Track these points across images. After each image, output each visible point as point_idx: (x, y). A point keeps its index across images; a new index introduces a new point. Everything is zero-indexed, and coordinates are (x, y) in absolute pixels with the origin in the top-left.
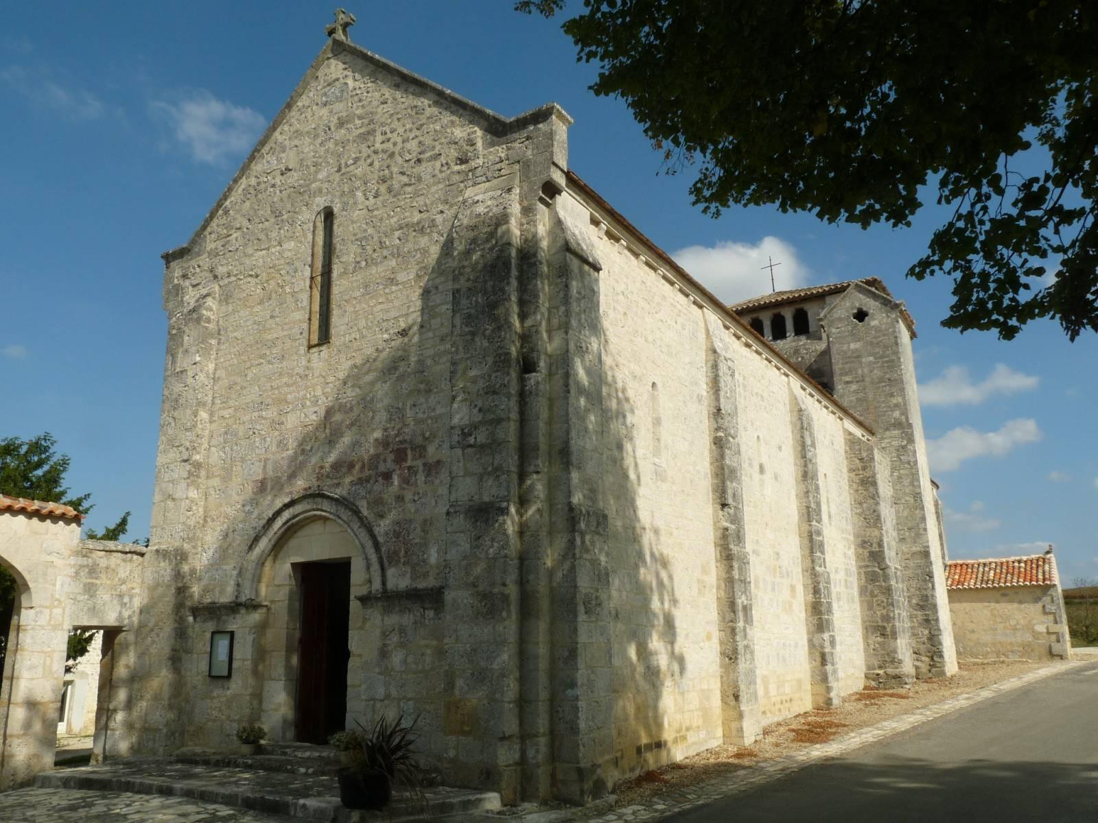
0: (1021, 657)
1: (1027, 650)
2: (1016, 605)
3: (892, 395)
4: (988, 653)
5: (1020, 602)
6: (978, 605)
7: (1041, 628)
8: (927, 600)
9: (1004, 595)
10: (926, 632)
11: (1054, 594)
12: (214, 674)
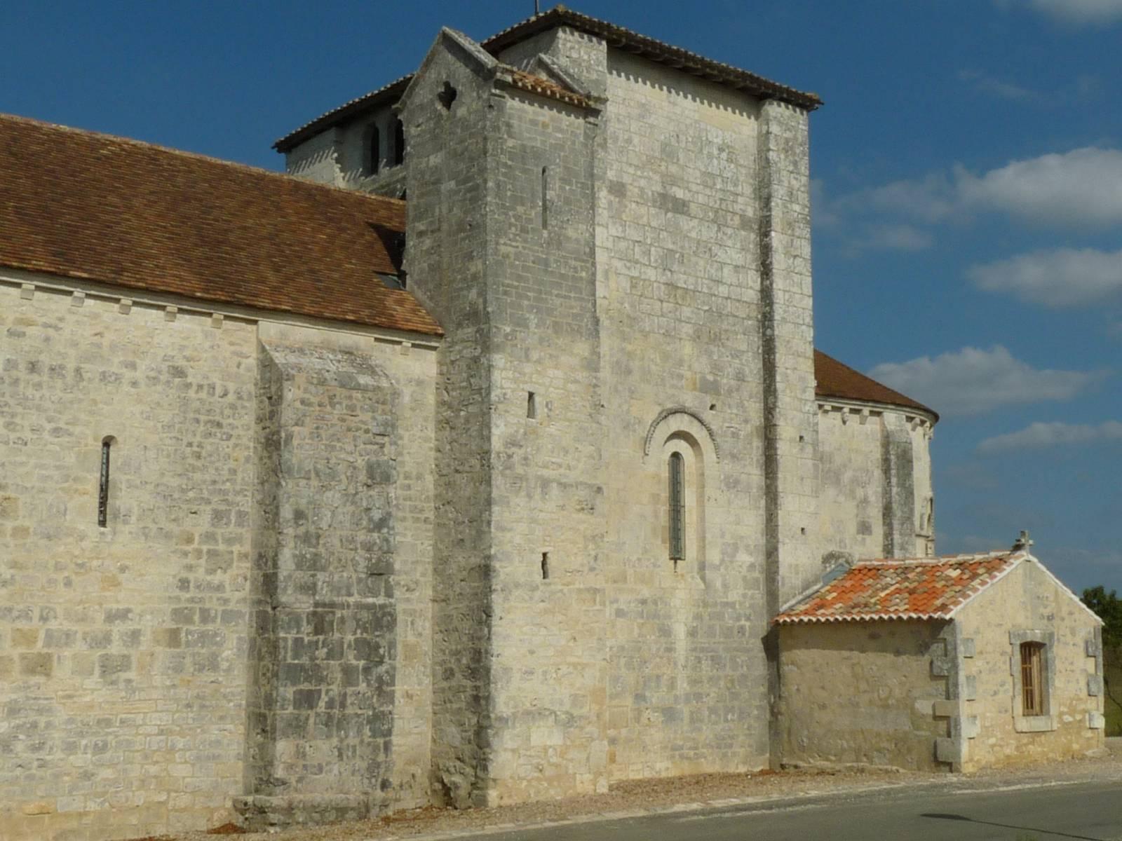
0: (891, 762)
1: (900, 748)
2: (890, 657)
3: (470, 257)
4: (843, 750)
5: (898, 653)
6: (833, 655)
7: (924, 707)
8: (479, 661)
9: (873, 637)
10: (474, 720)
11: (949, 638)
12: (937, 714)
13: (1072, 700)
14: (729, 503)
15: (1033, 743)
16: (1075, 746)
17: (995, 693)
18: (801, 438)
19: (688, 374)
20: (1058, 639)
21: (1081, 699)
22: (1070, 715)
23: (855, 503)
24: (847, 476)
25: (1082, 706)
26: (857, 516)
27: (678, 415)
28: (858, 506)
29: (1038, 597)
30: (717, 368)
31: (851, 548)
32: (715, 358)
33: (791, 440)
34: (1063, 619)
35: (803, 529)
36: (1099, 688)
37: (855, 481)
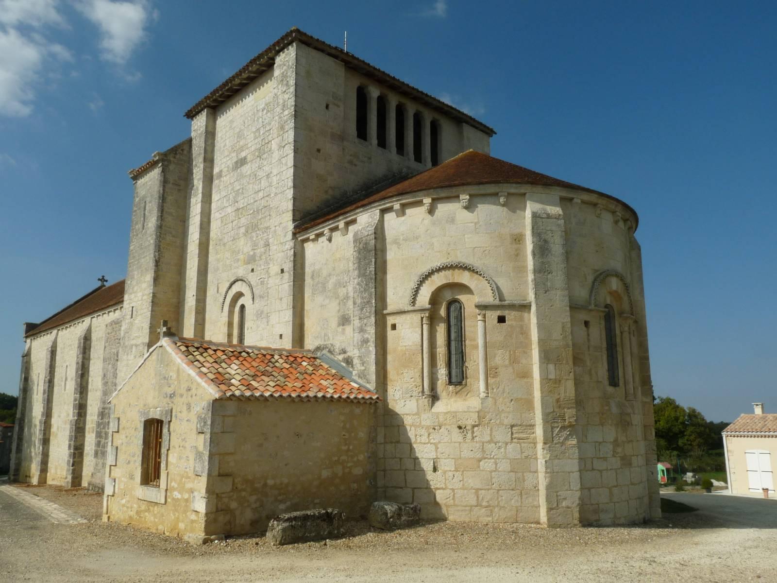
13: (182, 477)
15: (148, 510)
20: (176, 417)
21: (189, 478)
22: (179, 493)
23: (338, 301)
24: (330, 285)
25: (189, 485)
26: (339, 311)
27: (236, 283)
28: (339, 304)
29: (165, 378)
30: (255, 246)
31: (333, 339)
32: (254, 239)
33: (277, 274)
34: (182, 396)
35: (281, 336)
36: (203, 467)
37: (340, 284)
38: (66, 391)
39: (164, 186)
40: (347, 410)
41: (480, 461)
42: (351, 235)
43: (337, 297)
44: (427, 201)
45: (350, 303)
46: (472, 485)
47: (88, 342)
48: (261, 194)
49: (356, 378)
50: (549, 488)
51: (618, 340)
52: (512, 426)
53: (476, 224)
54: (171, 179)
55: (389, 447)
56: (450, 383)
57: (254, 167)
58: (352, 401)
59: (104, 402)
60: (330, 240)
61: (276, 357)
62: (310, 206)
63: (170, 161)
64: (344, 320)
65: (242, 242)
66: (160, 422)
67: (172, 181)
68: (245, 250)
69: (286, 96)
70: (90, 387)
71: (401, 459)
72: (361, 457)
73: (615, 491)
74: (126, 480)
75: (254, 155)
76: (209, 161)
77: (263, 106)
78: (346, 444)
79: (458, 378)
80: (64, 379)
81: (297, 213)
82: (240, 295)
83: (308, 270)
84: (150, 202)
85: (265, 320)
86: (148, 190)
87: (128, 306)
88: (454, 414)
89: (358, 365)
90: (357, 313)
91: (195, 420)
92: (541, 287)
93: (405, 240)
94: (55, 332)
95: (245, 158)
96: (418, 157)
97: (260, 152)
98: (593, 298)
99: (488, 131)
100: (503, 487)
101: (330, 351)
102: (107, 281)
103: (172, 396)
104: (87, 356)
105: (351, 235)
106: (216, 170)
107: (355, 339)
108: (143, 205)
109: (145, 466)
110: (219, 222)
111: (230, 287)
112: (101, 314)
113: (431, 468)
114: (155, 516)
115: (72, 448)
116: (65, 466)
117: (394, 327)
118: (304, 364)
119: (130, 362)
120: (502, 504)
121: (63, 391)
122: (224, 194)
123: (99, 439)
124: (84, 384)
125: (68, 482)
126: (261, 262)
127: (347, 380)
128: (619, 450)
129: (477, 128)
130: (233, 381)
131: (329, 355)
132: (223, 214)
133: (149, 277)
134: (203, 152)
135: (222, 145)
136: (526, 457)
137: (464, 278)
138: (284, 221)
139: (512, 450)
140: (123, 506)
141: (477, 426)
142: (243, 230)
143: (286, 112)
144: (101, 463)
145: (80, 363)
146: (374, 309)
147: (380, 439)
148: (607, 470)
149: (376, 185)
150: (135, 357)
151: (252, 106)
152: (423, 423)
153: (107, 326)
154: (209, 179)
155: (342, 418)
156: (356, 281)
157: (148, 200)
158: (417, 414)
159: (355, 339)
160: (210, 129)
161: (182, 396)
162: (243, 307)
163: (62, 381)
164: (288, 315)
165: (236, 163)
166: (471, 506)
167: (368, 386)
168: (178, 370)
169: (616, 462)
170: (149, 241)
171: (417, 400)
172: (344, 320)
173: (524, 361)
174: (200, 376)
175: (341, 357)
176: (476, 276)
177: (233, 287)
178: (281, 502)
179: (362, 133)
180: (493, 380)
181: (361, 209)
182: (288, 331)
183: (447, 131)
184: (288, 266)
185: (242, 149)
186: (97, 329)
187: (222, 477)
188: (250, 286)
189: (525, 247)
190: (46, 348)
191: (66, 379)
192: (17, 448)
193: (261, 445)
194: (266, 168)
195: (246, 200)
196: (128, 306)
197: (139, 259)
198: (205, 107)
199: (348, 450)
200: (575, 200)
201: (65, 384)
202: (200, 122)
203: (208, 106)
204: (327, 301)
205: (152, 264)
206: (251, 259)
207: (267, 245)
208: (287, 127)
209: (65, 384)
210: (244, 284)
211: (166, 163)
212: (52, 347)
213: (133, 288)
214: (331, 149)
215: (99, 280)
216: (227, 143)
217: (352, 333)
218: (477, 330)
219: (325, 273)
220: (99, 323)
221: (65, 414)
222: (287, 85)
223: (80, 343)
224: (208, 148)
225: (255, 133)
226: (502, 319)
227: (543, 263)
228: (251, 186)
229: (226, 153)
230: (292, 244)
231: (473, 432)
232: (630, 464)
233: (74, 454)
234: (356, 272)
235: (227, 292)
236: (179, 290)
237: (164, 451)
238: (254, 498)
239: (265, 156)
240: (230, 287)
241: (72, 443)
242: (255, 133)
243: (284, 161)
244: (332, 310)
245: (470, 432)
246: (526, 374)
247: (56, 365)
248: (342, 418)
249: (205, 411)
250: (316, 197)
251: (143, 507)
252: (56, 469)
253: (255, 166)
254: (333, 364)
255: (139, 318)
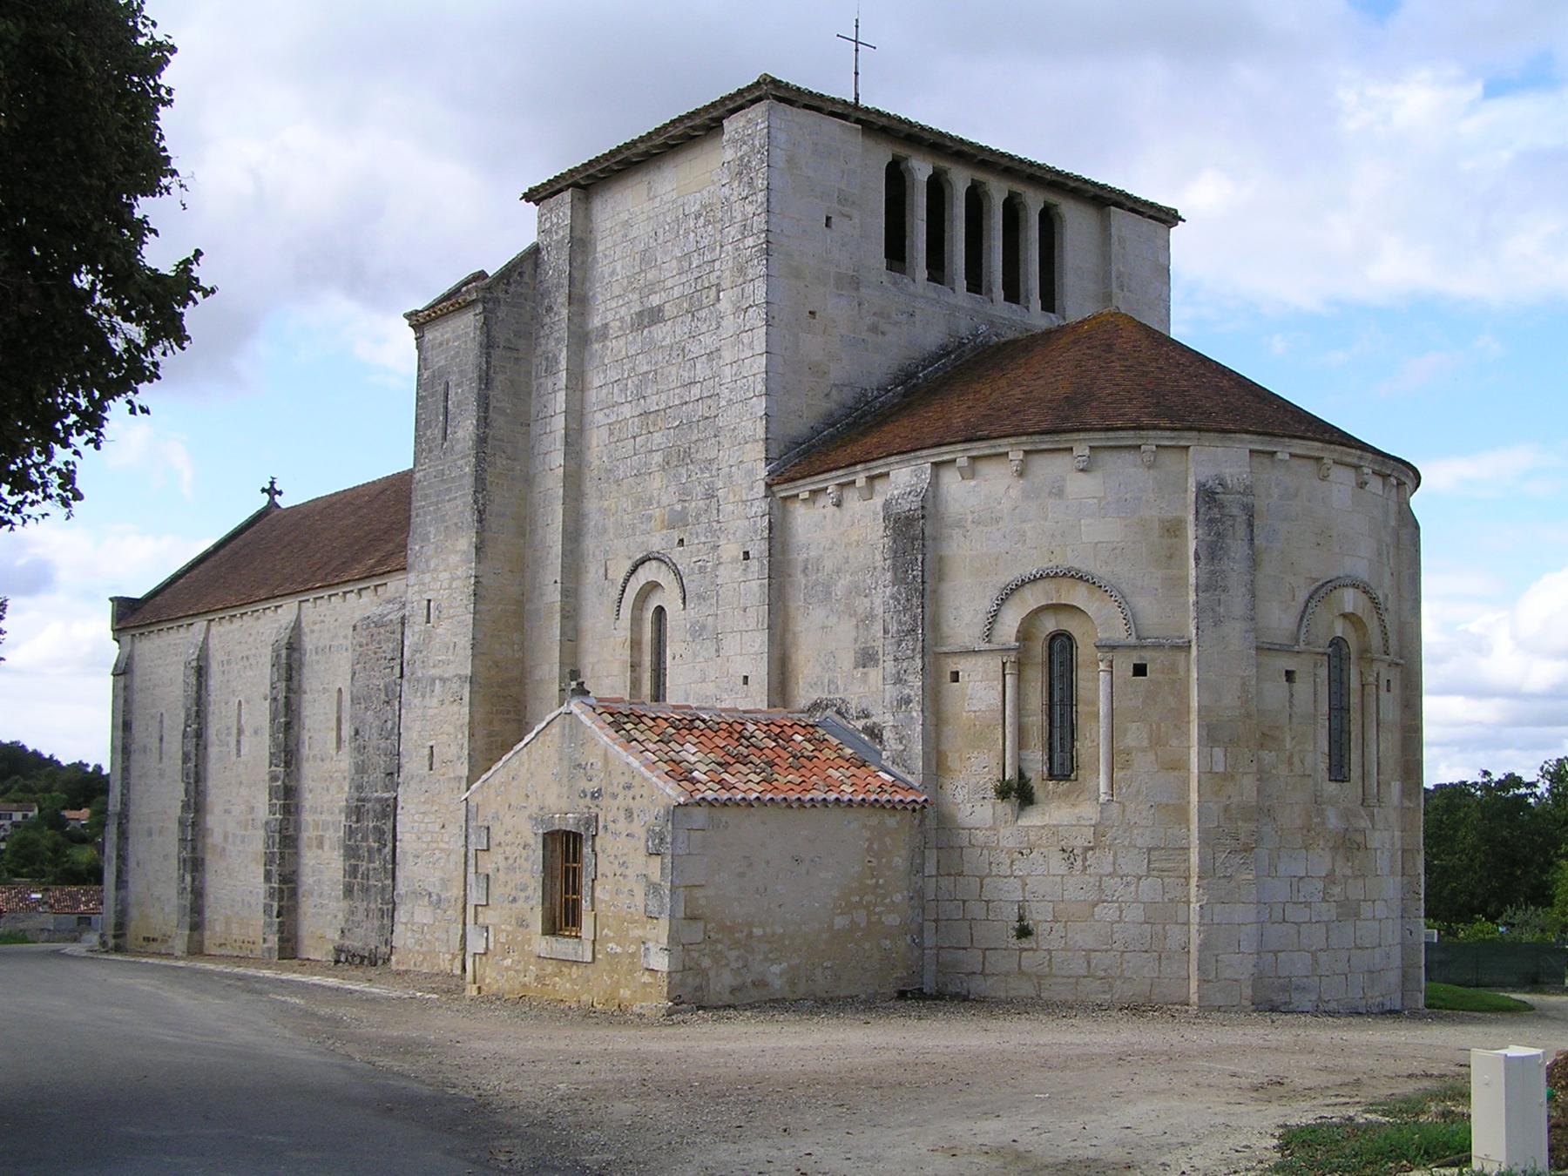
14: (695, 655)
15: (560, 974)
16: (625, 993)
17: (514, 900)
18: (746, 554)
19: (657, 512)
20: (605, 827)
25: (638, 932)
26: (856, 640)
30: (685, 494)
33: (734, 560)
34: (615, 796)
36: (662, 905)
37: (856, 590)
38: (243, 758)
39: (488, 355)
40: (873, 821)
41: (1095, 905)
42: (878, 501)
43: (853, 614)
44: (1016, 455)
45: (877, 628)
46: (1080, 943)
47: (296, 655)
48: (696, 391)
49: (888, 764)
50: (1203, 947)
51: (1355, 700)
52: (1150, 850)
53: (1100, 499)
54: (501, 337)
55: (945, 882)
56: (1051, 776)
57: (678, 332)
58: (883, 807)
59: (360, 788)
60: (838, 505)
61: (751, 727)
62: (799, 426)
63: (497, 301)
64: (867, 658)
65: (657, 482)
66: (577, 837)
67: (502, 344)
68: (665, 500)
69: (750, 209)
70: (305, 751)
71: (964, 902)
72: (898, 898)
73: (1322, 956)
74: (509, 928)
75: (679, 306)
76: (579, 301)
77: (697, 207)
78: (873, 876)
79: (1063, 767)
80: (234, 731)
81: (773, 445)
82: (653, 586)
83: (799, 557)
84: (458, 385)
85: (711, 647)
86: (453, 358)
87: (416, 598)
88: (1055, 829)
89: (892, 742)
90: (889, 648)
91: (641, 833)
92: (1209, 614)
93: (976, 523)
94: (200, 624)
95: (660, 309)
96: (1013, 292)
97: (691, 304)
98: (1304, 630)
99: (1164, 217)
100: (1131, 948)
101: (838, 712)
102: (280, 493)
103: (596, 795)
104: (294, 685)
105: (878, 501)
106: (596, 322)
107: (888, 696)
108: (441, 388)
109: (547, 905)
110: (604, 432)
111: (633, 571)
112: (325, 594)
113: (1278, 1087)
114: (574, 982)
115: (276, 878)
116: (260, 918)
117: (955, 677)
118: (798, 738)
119: (431, 712)
120: (1128, 974)
121: (234, 758)
122: (613, 375)
123: (353, 862)
124: (292, 745)
125: (269, 949)
126: (699, 529)
127: (873, 768)
128: (1337, 890)
129: (1141, 214)
130: (695, 774)
131: (837, 718)
132: (613, 418)
133: (465, 542)
134: (566, 282)
135: (607, 270)
136: (1171, 900)
137: (1077, 596)
138: (745, 462)
139: (1149, 888)
140: (508, 968)
141: (1092, 849)
142: (658, 458)
143: (750, 242)
144: (361, 909)
145: (282, 701)
146: (920, 645)
147: (930, 868)
148: (1310, 922)
149: (925, 368)
150: (442, 702)
151: (674, 202)
152: (1003, 843)
153: (355, 628)
154: (581, 339)
155: (867, 834)
156: (888, 591)
157: (453, 379)
158: (993, 828)
159: (888, 696)
160: (578, 234)
161: (615, 796)
162: (660, 611)
163: (229, 734)
164: (760, 641)
165: (640, 314)
166: (1078, 977)
167: (909, 778)
168: (606, 755)
169: (1328, 911)
170: (461, 468)
171: (994, 806)
172: (867, 658)
173: (1174, 742)
174: (646, 766)
175: (860, 724)
176: (1098, 594)
177: (640, 570)
178: (773, 962)
179: (896, 252)
180: (1121, 774)
181: (898, 458)
182: (760, 672)
183: (1076, 221)
184: (758, 548)
185: (651, 288)
186: (316, 628)
187: (693, 923)
188: (677, 573)
189: (1186, 545)
190: (183, 658)
191: (240, 732)
192: (118, 877)
193: (742, 875)
194: (706, 339)
195: (664, 397)
196: (416, 598)
197: (437, 503)
198: (568, 187)
199: (877, 885)
200: (1280, 456)
201: (238, 742)
202: (557, 216)
203: (576, 185)
204: (833, 620)
205: (469, 517)
206: (677, 520)
207: (710, 495)
208: (751, 273)
209: (238, 742)
210: (664, 567)
211: (490, 305)
212: (198, 659)
213: (427, 561)
214: (836, 308)
215: (263, 490)
216: (619, 269)
217: (880, 682)
218: (1097, 687)
219: (828, 565)
220: (334, 620)
221: (243, 807)
222: (751, 184)
223: (278, 656)
224: (575, 274)
225: (679, 260)
226: (1140, 670)
227: (1213, 573)
228: (674, 370)
229: (617, 290)
230: (763, 506)
231: (1085, 859)
232: (1357, 915)
233: (281, 891)
234: (889, 575)
235: (627, 581)
236: (522, 565)
237: (586, 881)
238: (734, 953)
239: (703, 314)
240: (633, 571)
241: (274, 868)
242: (679, 260)
243: (745, 337)
244: (844, 637)
245: (1079, 860)
246: (1177, 765)
247: (211, 699)
248: (867, 834)
249: (661, 821)
250: (807, 412)
251: (549, 969)
252: (228, 923)
253: (681, 330)
254: (848, 737)
255: (445, 624)
